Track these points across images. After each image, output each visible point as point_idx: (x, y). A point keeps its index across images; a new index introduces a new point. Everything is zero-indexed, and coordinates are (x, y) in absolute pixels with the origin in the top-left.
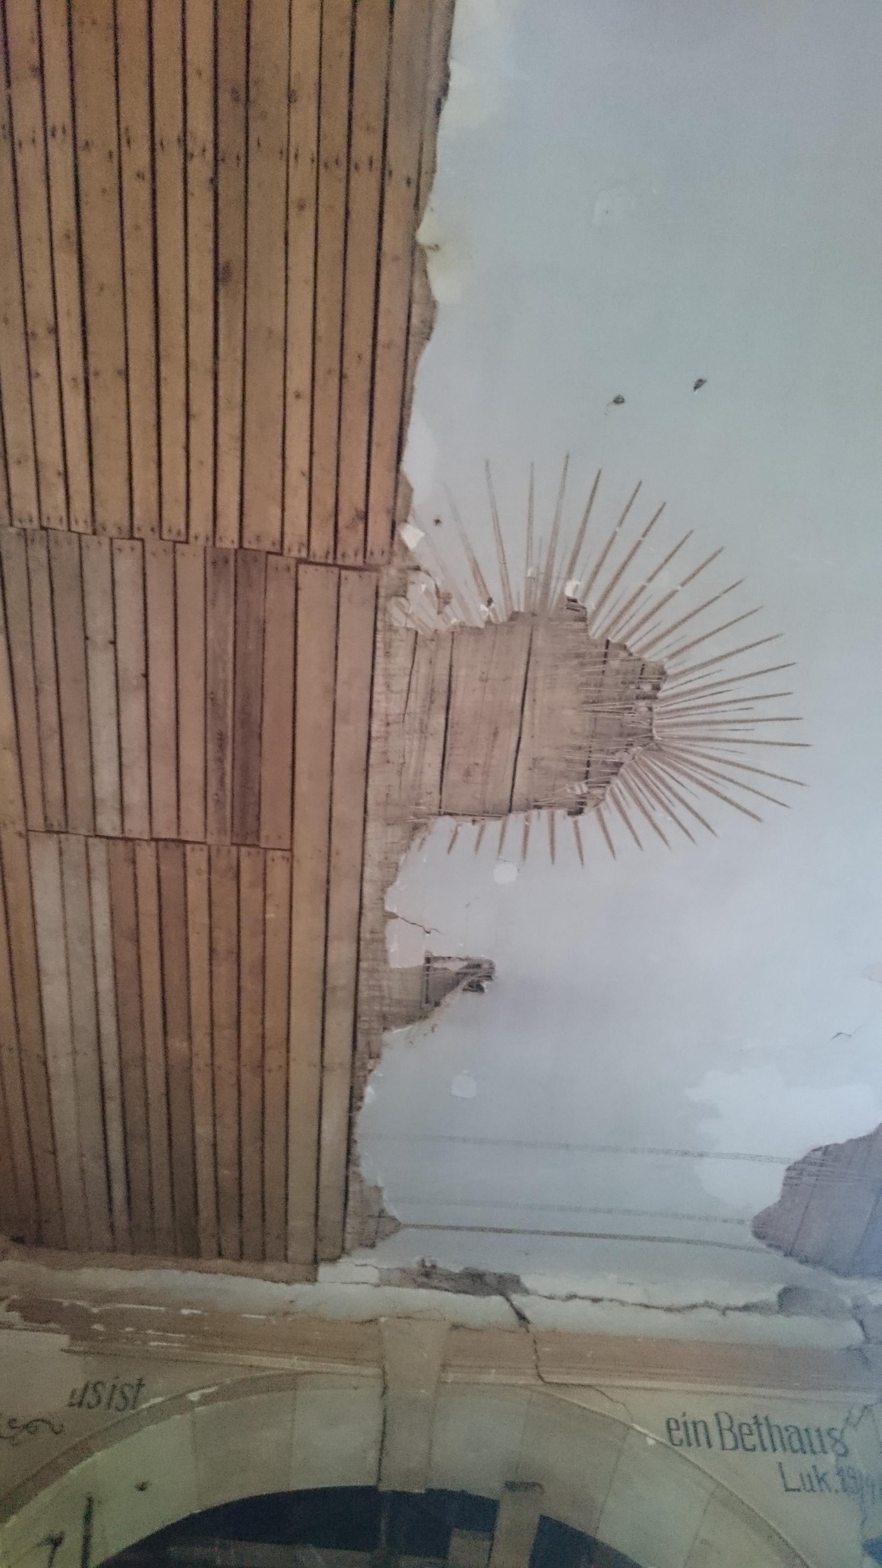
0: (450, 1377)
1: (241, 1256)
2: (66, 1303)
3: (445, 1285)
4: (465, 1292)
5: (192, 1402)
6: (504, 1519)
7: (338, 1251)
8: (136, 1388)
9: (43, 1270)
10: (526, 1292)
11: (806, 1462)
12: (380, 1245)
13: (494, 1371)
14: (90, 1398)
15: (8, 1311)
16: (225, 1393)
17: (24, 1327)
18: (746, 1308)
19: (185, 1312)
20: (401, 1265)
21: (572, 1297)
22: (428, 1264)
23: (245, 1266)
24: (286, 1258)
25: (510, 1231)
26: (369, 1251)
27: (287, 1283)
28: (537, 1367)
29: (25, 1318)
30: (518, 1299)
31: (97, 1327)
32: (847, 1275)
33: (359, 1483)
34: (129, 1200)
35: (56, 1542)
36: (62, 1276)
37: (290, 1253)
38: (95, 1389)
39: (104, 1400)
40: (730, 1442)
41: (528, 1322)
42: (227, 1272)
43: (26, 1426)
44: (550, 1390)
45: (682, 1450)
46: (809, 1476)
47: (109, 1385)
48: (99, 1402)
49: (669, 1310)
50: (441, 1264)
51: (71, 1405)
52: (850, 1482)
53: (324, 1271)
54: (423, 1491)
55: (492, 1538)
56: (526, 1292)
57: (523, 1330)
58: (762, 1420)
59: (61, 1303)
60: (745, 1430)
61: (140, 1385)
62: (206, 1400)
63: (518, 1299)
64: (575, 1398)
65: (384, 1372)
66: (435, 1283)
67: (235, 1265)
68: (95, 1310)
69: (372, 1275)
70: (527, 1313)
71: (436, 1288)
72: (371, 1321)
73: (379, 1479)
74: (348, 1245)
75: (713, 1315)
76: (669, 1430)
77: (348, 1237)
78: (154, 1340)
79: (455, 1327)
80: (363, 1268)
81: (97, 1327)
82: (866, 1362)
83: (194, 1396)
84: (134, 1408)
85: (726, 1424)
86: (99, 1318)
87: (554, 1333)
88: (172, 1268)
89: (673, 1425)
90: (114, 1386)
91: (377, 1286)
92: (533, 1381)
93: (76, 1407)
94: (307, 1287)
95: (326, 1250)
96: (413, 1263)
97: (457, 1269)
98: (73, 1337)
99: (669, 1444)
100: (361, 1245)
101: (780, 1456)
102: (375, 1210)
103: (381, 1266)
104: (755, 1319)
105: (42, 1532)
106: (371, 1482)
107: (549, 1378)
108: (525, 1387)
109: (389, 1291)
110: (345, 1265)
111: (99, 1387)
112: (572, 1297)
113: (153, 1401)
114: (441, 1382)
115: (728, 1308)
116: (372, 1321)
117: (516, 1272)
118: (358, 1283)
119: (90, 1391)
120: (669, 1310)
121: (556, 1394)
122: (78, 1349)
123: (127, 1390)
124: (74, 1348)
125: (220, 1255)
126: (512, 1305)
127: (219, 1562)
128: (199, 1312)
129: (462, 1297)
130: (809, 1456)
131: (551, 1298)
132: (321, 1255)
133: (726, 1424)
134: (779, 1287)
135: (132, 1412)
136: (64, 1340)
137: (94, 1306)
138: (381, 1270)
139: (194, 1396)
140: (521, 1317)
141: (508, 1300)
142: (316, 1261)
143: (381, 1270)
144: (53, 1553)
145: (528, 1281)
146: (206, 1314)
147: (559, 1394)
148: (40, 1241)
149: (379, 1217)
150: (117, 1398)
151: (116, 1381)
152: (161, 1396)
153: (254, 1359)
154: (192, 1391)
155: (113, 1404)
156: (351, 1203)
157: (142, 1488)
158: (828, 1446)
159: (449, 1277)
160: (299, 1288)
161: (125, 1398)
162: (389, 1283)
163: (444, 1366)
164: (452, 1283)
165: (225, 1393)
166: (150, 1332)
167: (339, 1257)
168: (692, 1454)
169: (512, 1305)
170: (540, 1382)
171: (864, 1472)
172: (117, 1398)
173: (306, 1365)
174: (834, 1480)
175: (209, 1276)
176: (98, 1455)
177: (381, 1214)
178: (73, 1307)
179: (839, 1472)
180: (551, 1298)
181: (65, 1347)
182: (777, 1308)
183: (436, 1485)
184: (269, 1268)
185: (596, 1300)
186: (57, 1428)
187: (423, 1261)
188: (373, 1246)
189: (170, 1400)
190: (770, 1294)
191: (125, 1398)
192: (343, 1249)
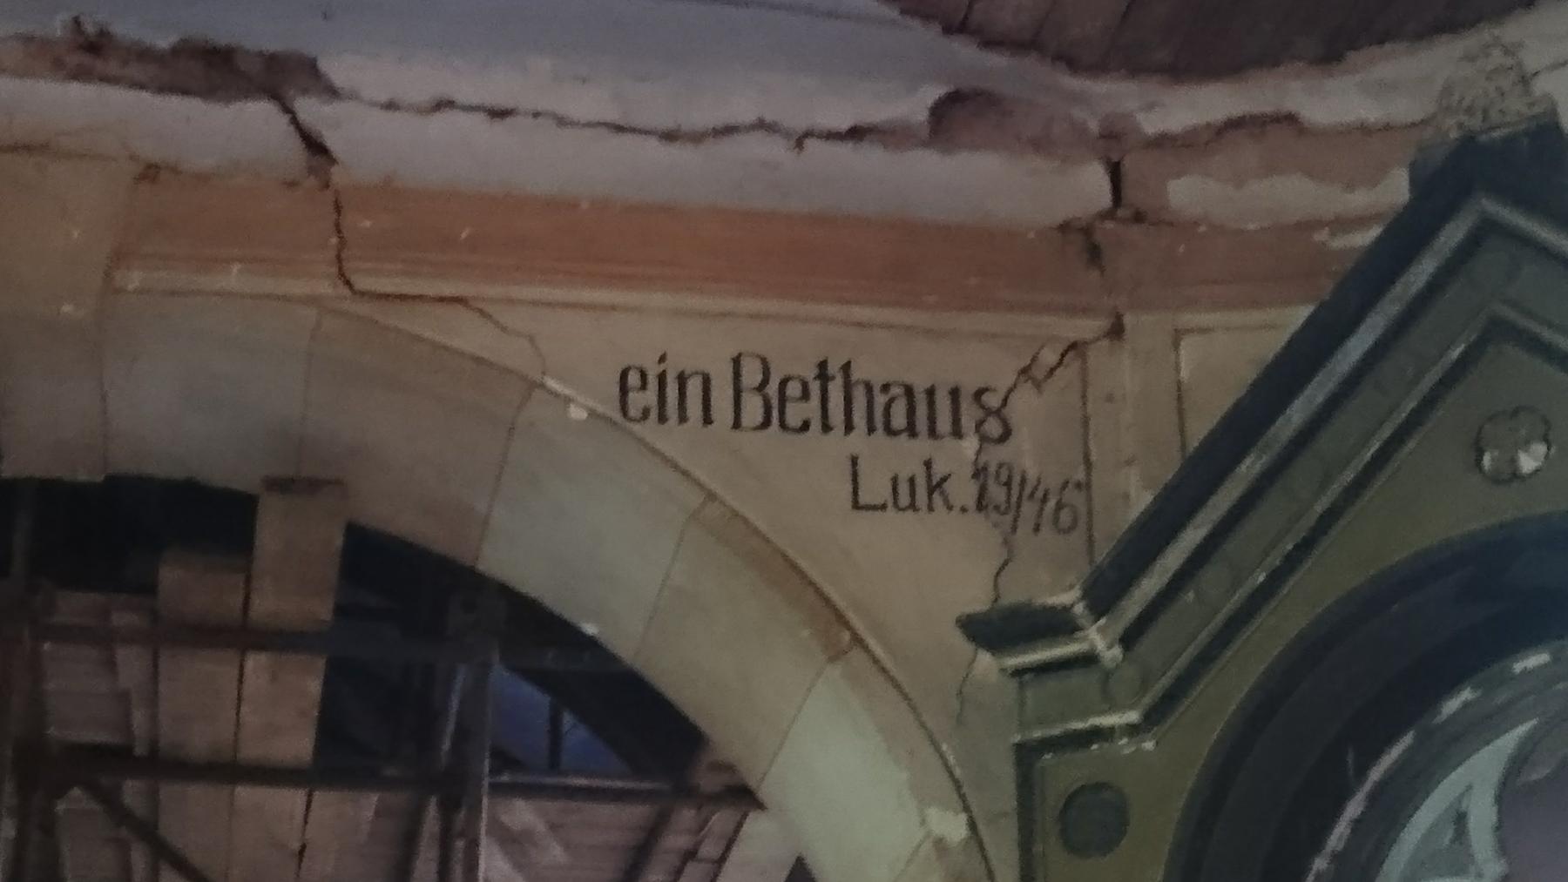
0: (134, 279)
11: (907, 456)
18: (856, 134)
21: (443, 105)
30: (310, 109)
32: (1098, 69)
40: (753, 409)
45: (648, 430)
46: (912, 481)
49: (670, 136)
52: (997, 493)
56: (332, 93)
58: (834, 368)
60: (794, 389)
63: (310, 109)
64: (426, 325)
66: (112, 67)
70: (332, 141)
75: (774, 150)
76: (624, 390)
82: (1094, 254)
85: (752, 375)
87: (388, 193)
89: (634, 379)
92: (325, 287)
97: (164, 42)
99: (617, 416)
101: (838, 445)
104: (870, 159)
107: (363, 282)
112: (443, 105)
115: (808, 134)
120: (670, 136)
130: (922, 446)
131: (391, 106)
133: (752, 375)
134: (932, 93)
140: (315, 146)
141: (288, 110)
145: (336, 69)
158: (967, 423)
163: (120, 257)
168: (672, 439)
171: (1032, 475)
174: (963, 490)
179: (979, 472)
180: (391, 106)
182: (925, 133)
185: (499, 113)
190: (915, 106)
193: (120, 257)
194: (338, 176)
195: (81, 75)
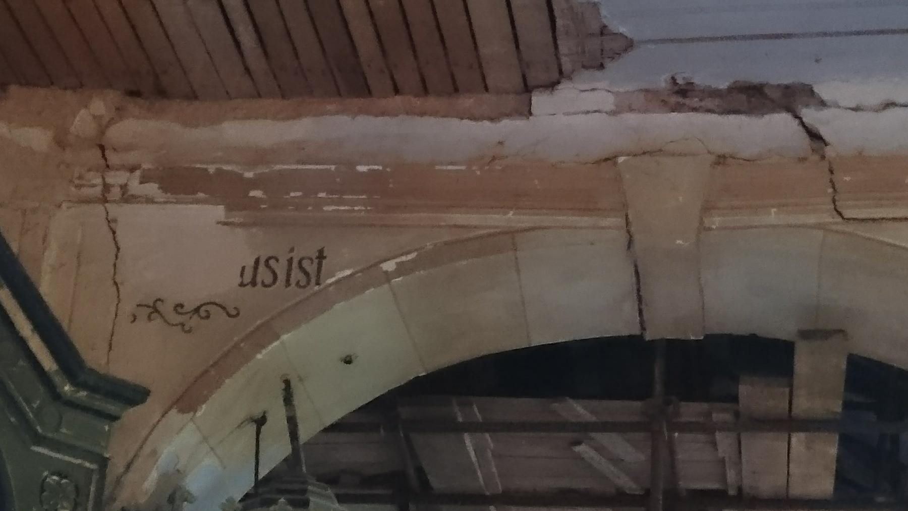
0: (716, 221)
1: (425, 90)
2: (212, 169)
3: (709, 103)
4: (736, 112)
5: (386, 272)
6: (802, 364)
7: (556, 75)
8: (316, 261)
9: (177, 128)
10: (823, 104)
12: (609, 65)
13: (773, 210)
14: (264, 275)
15: (141, 183)
16: (428, 260)
17: (165, 200)
19: (362, 168)
20: (644, 85)
21: (889, 105)
22: (680, 81)
23: (432, 102)
24: (486, 89)
25: (789, 36)
26: (598, 74)
27: (492, 119)
28: (834, 201)
29: (164, 189)
30: (810, 115)
31: (256, 193)
33: (625, 332)
34: (261, 40)
35: (260, 422)
36: (202, 134)
37: (489, 82)
38: (267, 265)
39: (281, 277)
41: (826, 144)
42: (410, 112)
43: (197, 310)
44: (850, 228)
47: (283, 262)
48: (275, 278)
50: (697, 80)
51: (242, 285)
53: (539, 100)
54: (702, 338)
55: (791, 386)
56: (823, 104)
57: (816, 158)
59: (206, 170)
61: (321, 256)
62: (402, 269)
63: (810, 115)
64: (888, 235)
65: (628, 223)
66: (695, 102)
67: (417, 102)
68: (249, 175)
69: (608, 101)
70: (824, 132)
71: (695, 110)
72: (606, 160)
73: (643, 328)
74: (567, 66)
77: (564, 60)
78: (329, 204)
79: (721, 160)
80: (592, 93)
81: (256, 193)
83: (389, 266)
84: (318, 284)
86: (254, 184)
88: (337, 113)
90: (290, 261)
91: (613, 113)
92: (828, 218)
93: (249, 287)
94: (518, 124)
95: (537, 75)
96: (662, 82)
97: (723, 85)
98: (230, 209)
100: (584, 67)
102: (595, 27)
103: (616, 89)
105: (241, 413)
106: (636, 331)
107: (848, 214)
108: (819, 226)
109: (631, 119)
110: (566, 90)
111: (272, 263)
112: (889, 105)
113: (341, 275)
114: (703, 229)
116: (611, 159)
117: (807, 81)
118: (588, 112)
119: (262, 268)
121: (859, 233)
122: (236, 220)
123: (305, 264)
124: (231, 220)
125: (397, 91)
126: (803, 124)
127: (460, 419)
128: (380, 168)
129: (732, 118)
131: (856, 109)
132: (531, 82)
135: (317, 288)
136: (219, 211)
137: (249, 171)
138: (617, 94)
139: (389, 266)
140: (814, 136)
142: (528, 89)
143: (617, 94)
144: (258, 433)
145: (823, 91)
146: (388, 170)
147: (862, 231)
148: (162, 93)
149: (602, 34)
150: (296, 274)
151: (292, 255)
152: (348, 268)
153: (459, 218)
154: (385, 260)
155: (293, 281)
156: (559, 22)
157: (348, 361)
159: (714, 93)
160: (507, 125)
161: (307, 274)
162: (631, 110)
163: (708, 208)
164: (717, 101)
165: (428, 260)
166: (322, 195)
167: (559, 83)
169: (803, 124)
170: (839, 220)
172: (296, 274)
173: (523, 220)
175: (387, 118)
176: (285, 337)
177: (603, 31)
178: (219, 172)
180: (856, 109)
181: (223, 219)
183: (716, 330)
184: (467, 102)
186: (234, 312)
187: (673, 79)
188: (601, 66)
189: (361, 271)
191: (307, 274)
192: (561, 72)
193: (708, 208)
194: (829, 152)
195: (677, 108)
